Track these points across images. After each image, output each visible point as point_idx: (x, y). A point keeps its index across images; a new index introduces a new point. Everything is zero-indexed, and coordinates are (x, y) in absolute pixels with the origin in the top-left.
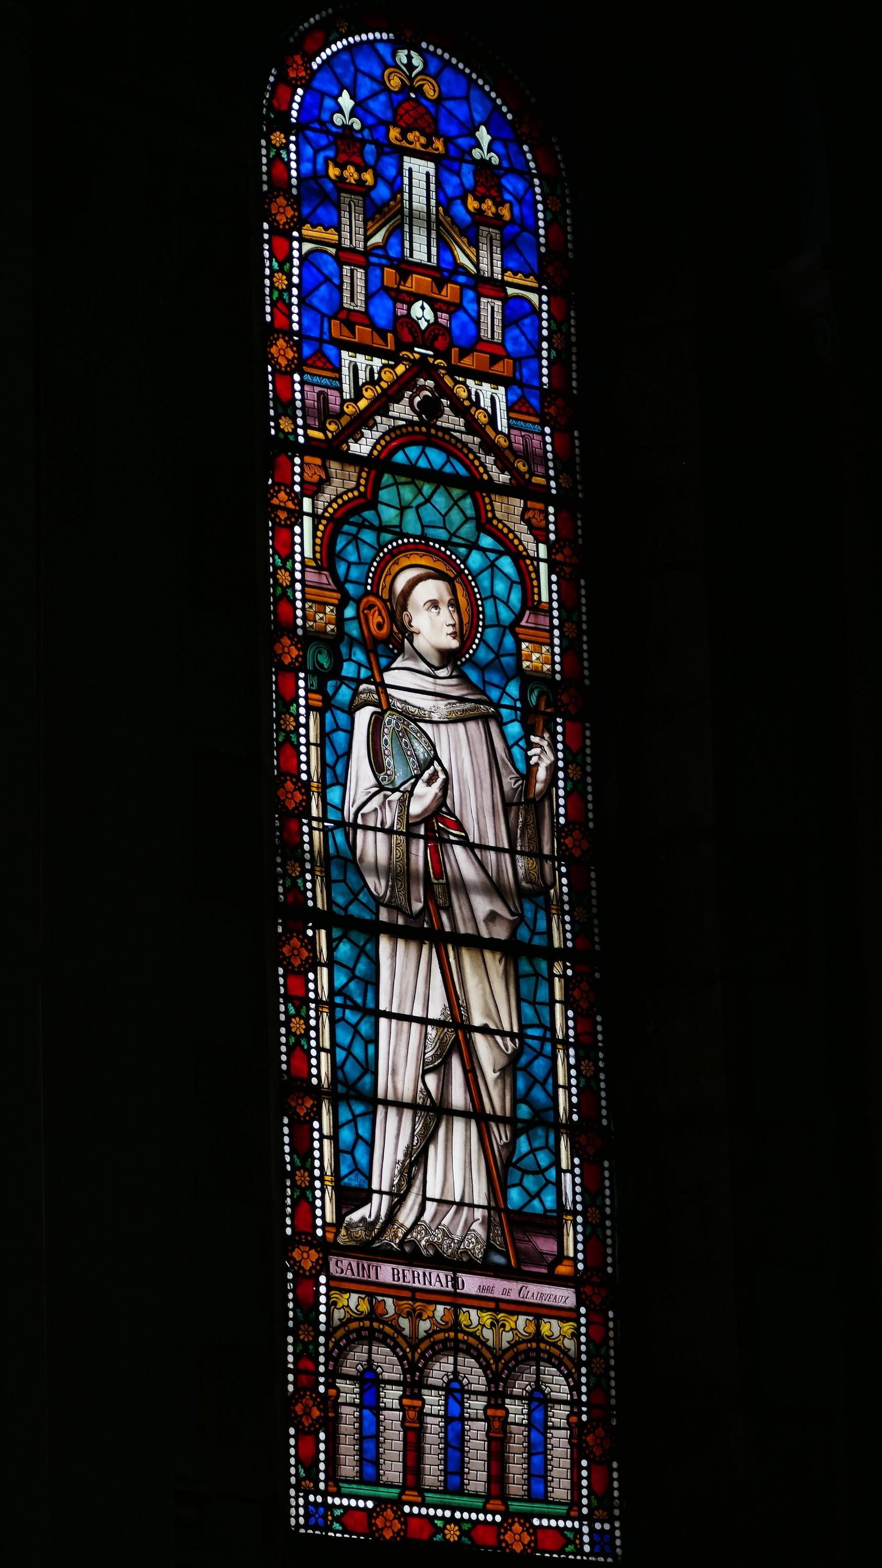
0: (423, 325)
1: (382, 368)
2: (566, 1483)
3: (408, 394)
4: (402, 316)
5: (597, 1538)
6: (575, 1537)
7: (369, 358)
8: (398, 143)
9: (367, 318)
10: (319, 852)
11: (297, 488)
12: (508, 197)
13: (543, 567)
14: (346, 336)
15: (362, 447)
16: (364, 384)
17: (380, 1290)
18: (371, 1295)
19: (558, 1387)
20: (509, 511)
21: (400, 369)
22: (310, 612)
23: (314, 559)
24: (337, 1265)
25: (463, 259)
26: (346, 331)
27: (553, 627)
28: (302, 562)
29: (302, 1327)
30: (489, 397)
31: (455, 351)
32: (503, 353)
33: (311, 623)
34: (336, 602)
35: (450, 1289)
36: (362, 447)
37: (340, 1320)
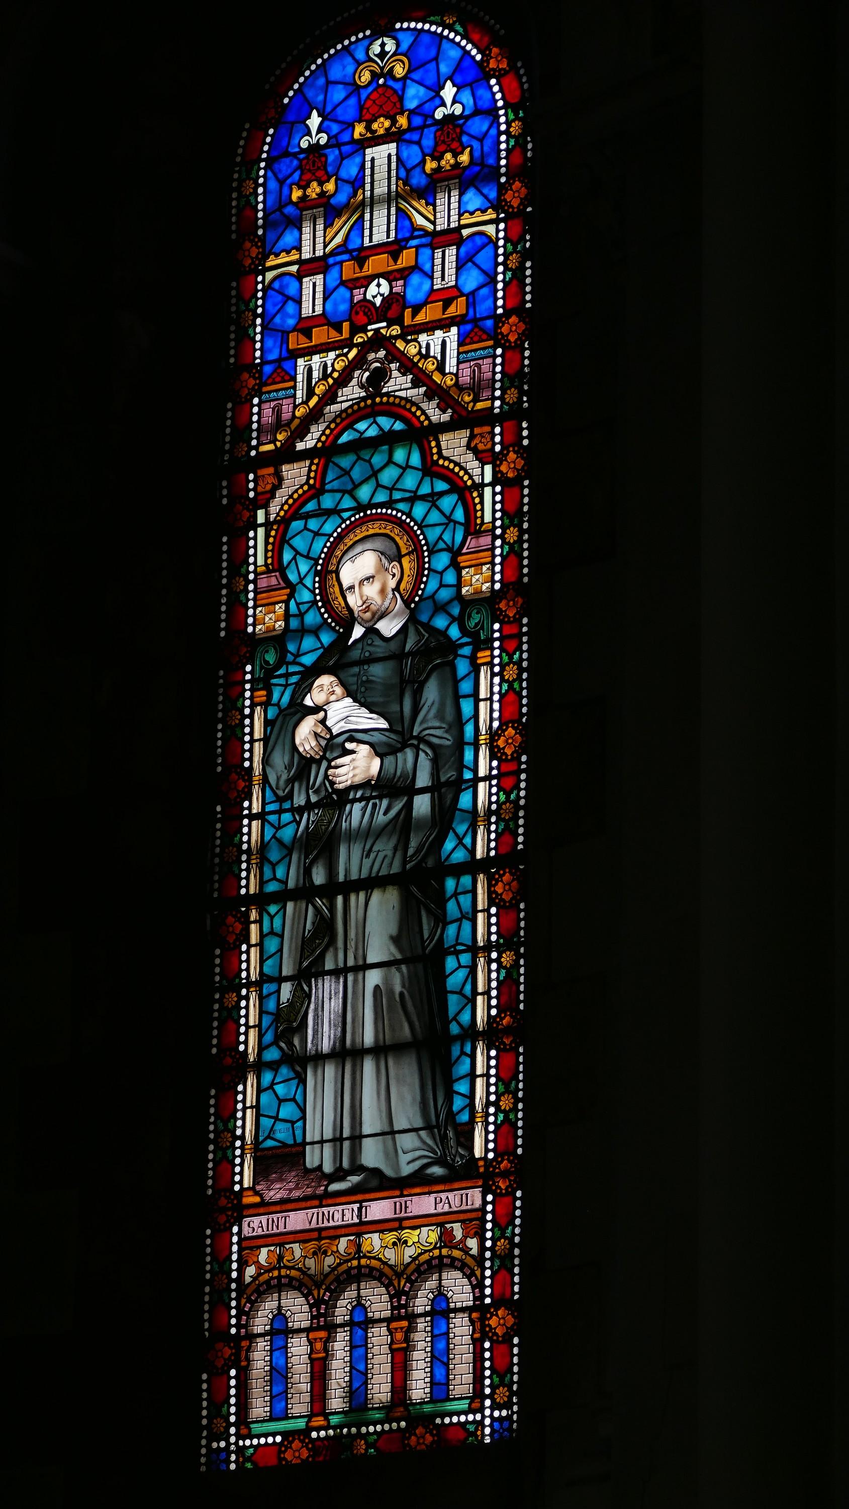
0: (378, 301)
1: (335, 360)
2: (469, 1378)
5: (496, 1425)
6: (476, 1429)
9: (324, 319)
10: (257, 841)
14: (304, 343)
15: (308, 443)
16: (316, 383)
17: (447, 1218)
18: (441, 1225)
19: (459, 1289)
20: (454, 446)
22: (259, 616)
23: (266, 565)
24: (249, 1226)
25: (420, 221)
26: (302, 339)
30: (440, 343)
35: (356, 1220)
36: (308, 443)
37: (329, 1266)
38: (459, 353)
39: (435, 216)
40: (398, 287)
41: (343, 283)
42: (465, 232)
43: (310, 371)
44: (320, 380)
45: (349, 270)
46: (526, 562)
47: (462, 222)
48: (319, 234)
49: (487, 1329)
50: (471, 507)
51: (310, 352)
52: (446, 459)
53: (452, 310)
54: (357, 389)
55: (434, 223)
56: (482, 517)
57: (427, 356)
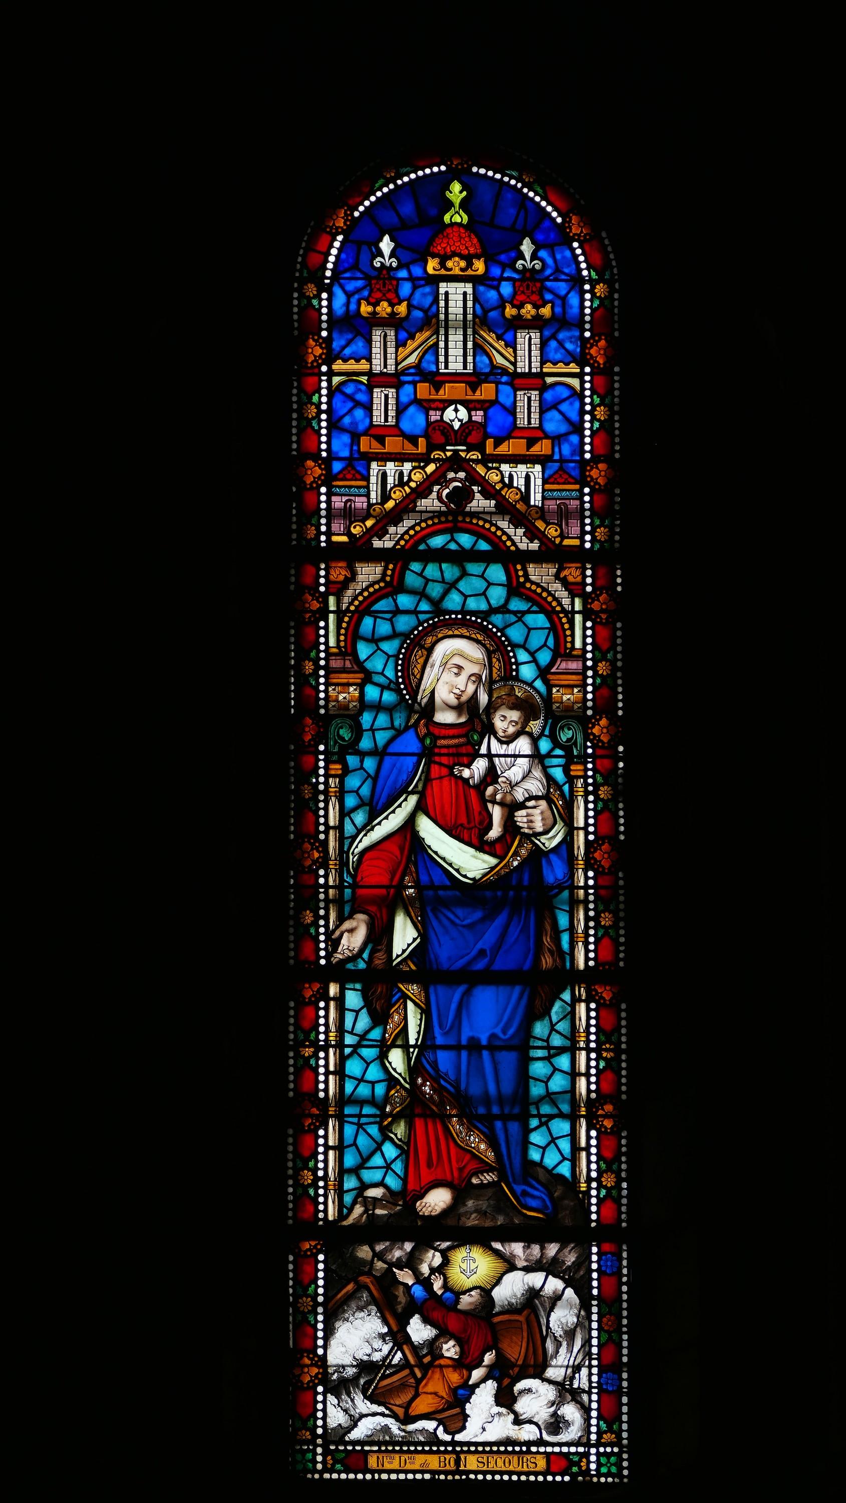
0: (457, 425)
1: (411, 471)
3: (436, 488)
4: (437, 421)
7: (383, 463)
8: (437, 273)
11: (322, 589)
12: (548, 297)
13: (578, 618)
14: (376, 448)
16: (391, 489)
21: (431, 468)
22: (332, 693)
23: (338, 647)
25: (499, 360)
26: (375, 444)
27: (586, 668)
28: (326, 651)
29: (310, 1308)
30: (524, 476)
31: (490, 442)
32: (541, 435)
33: (333, 704)
34: (359, 681)
38: (544, 490)
39: (515, 357)
40: (478, 416)
41: (416, 401)
42: (549, 380)
43: (384, 476)
44: (395, 486)
45: (424, 391)
46: (619, 633)
47: (545, 370)
48: (391, 350)
49: (589, 479)
50: (561, 633)
51: (383, 458)
52: (533, 583)
53: (536, 449)
54: (436, 503)
55: (514, 364)
56: (573, 642)
57: (510, 485)
